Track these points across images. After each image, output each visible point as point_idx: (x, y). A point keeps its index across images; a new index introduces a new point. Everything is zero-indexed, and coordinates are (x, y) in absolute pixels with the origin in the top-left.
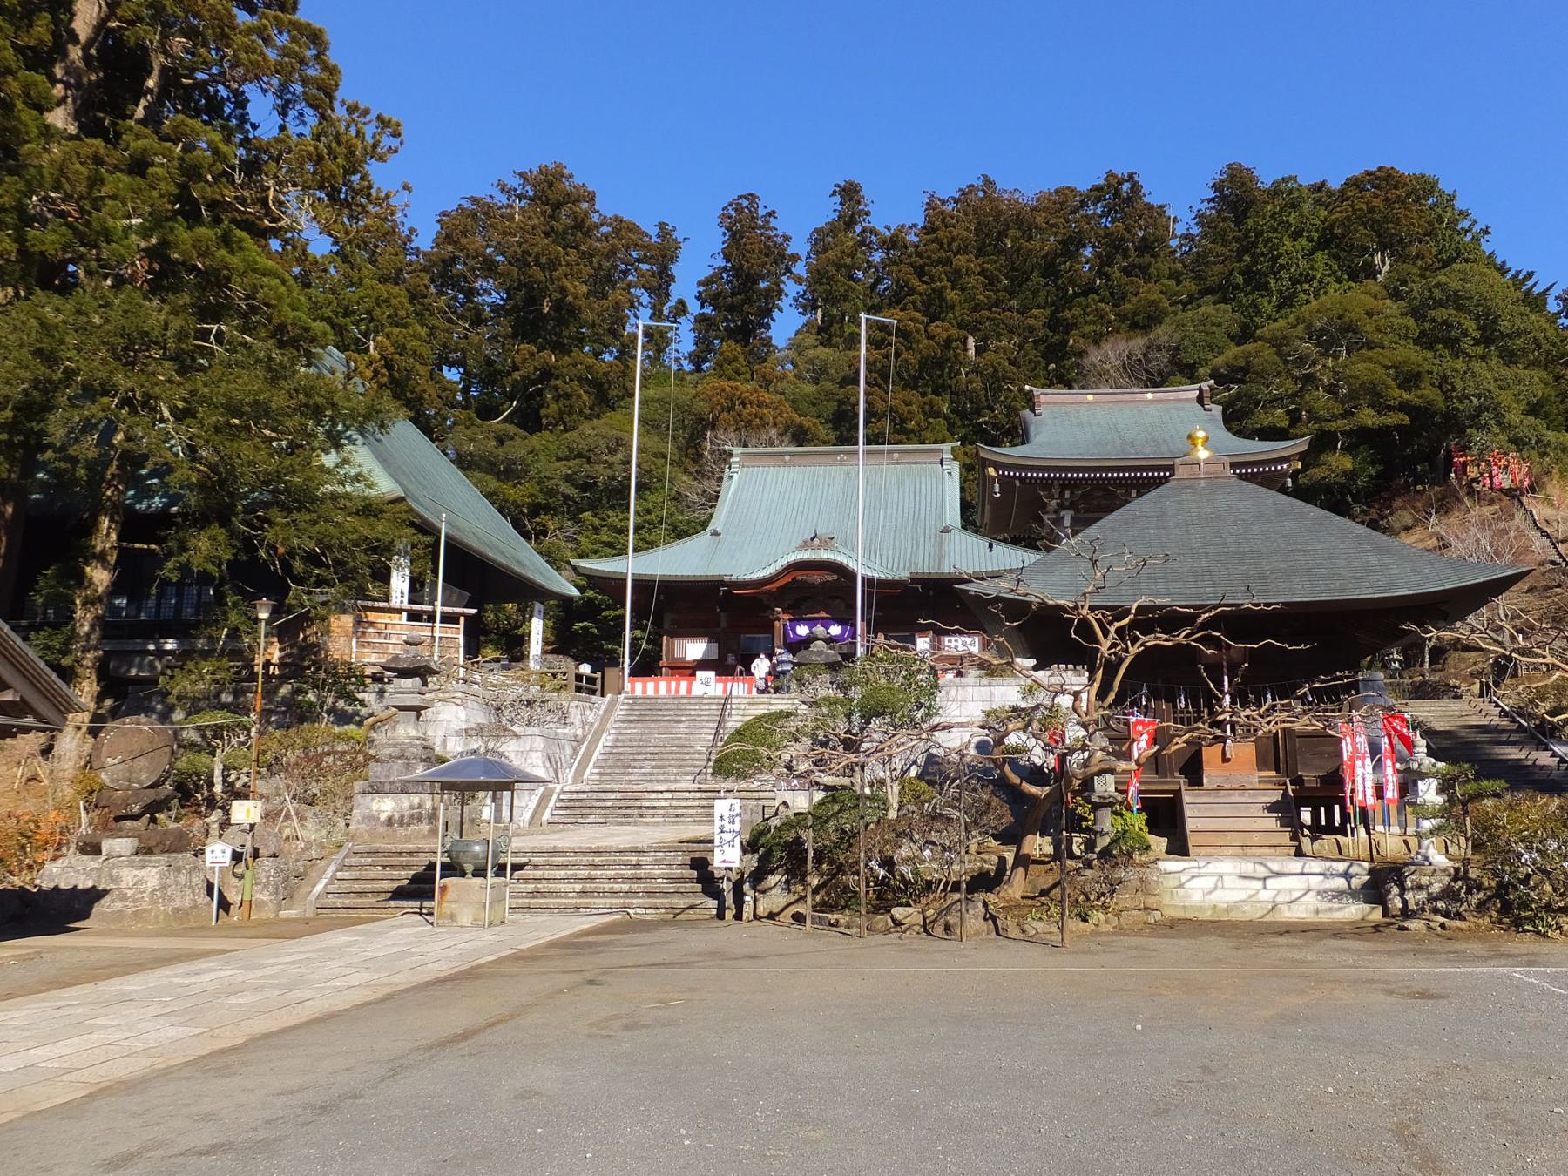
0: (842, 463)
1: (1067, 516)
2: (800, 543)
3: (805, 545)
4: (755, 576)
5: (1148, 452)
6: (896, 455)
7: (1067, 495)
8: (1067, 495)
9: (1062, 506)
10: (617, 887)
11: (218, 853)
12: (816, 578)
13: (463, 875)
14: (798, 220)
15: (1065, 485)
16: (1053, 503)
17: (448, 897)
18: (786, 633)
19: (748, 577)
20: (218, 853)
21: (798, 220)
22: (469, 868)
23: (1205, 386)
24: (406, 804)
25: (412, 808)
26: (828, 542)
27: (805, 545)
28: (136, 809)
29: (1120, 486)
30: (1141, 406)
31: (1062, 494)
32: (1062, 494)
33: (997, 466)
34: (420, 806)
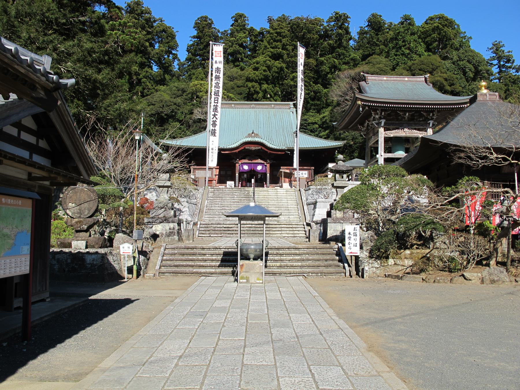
0: (253, 108)
1: (383, 122)
2: (246, 135)
3: (249, 135)
4: (230, 147)
5: (416, 98)
6: (273, 106)
7: (383, 114)
8: (383, 114)
9: (380, 118)
10: (295, 264)
11: (126, 248)
12: (253, 148)
13: (249, 259)
14: (223, 24)
15: (384, 109)
16: (377, 117)
17: (244, 270)
18: (240, 168)
19: (228, 147)
20: (126, 248)
21: (223, 24)
22: (252, 256)
23: (426, 76)
24: (168, 228)
25: (170, 229)
26: (257, 135)
27: (249, 135)
28: (85, 227)
29: (401, 111)
30: (404, 82)
31: (381, 113)
32: (381, 113)
33: (362, 100)
34: (174, 229)
